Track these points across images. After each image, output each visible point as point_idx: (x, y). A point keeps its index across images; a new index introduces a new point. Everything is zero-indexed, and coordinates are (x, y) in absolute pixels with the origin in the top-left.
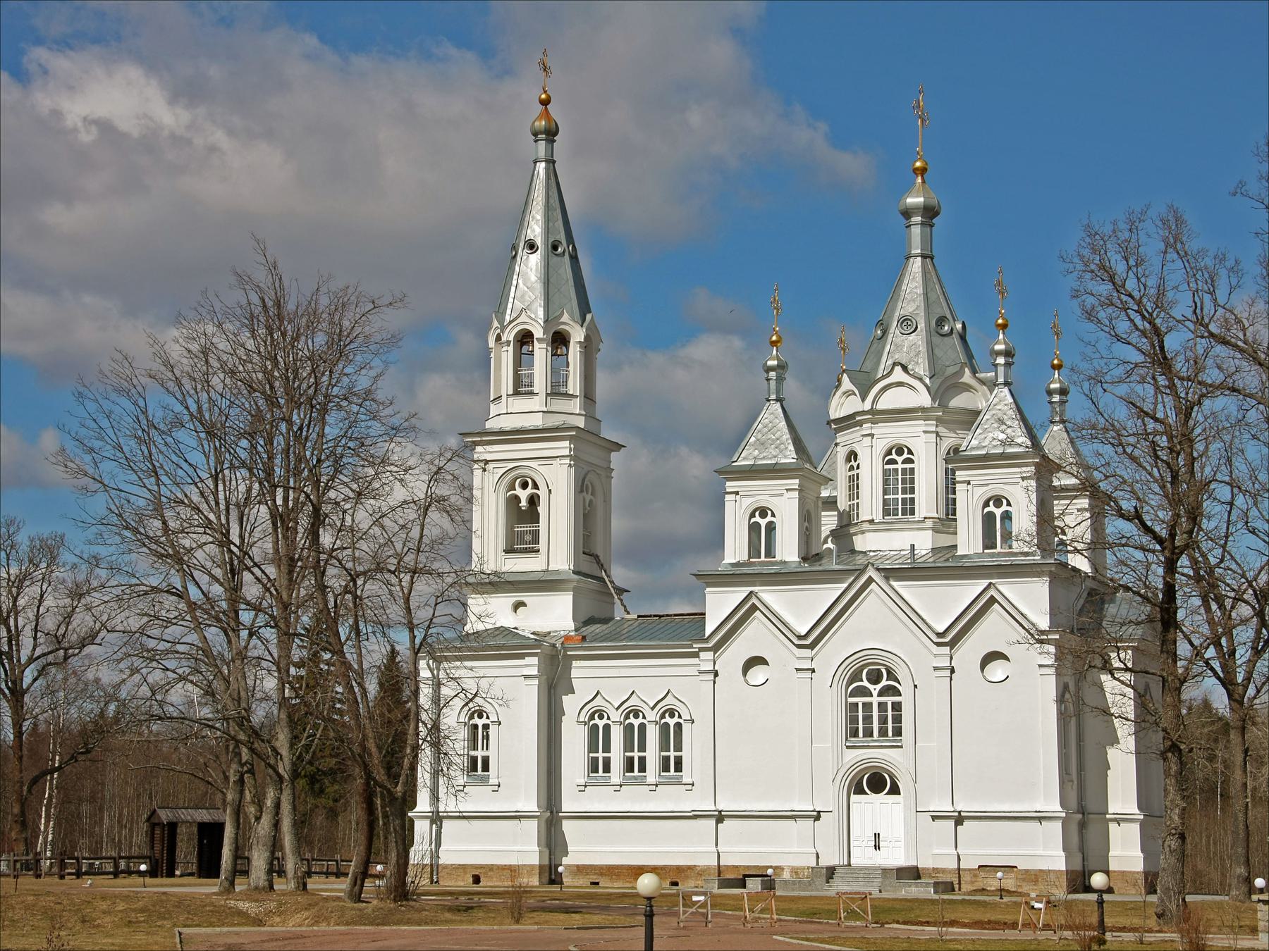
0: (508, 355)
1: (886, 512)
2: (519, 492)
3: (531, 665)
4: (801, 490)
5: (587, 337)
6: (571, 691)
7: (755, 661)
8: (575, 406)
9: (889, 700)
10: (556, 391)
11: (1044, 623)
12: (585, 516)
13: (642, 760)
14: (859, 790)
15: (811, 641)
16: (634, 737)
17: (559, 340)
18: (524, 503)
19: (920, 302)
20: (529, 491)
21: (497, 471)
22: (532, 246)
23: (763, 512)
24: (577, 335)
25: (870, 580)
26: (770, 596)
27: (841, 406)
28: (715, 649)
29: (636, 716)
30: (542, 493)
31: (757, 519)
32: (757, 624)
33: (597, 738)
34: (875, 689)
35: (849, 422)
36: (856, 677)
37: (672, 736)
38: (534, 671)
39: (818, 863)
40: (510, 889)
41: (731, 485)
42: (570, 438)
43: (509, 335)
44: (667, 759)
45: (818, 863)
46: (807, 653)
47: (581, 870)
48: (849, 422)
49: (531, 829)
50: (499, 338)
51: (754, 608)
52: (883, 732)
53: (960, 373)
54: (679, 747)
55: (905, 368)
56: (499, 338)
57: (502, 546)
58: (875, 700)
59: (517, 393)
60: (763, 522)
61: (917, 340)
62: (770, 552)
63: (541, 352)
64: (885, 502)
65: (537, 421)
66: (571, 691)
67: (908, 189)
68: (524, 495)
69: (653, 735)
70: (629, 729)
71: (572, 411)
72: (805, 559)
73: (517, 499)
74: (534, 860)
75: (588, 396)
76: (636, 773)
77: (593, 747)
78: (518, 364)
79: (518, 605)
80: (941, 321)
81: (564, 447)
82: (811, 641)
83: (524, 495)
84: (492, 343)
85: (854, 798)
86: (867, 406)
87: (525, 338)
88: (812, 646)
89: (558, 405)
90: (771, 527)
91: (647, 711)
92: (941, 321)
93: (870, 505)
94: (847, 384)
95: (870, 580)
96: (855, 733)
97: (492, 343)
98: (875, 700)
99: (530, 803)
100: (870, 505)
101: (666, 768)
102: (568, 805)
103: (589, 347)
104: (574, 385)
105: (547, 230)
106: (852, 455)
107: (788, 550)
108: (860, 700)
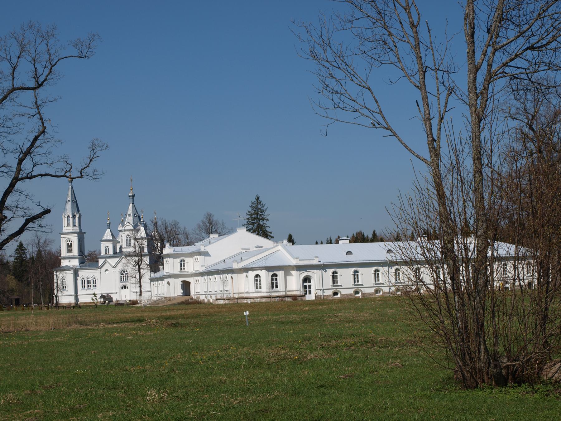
0: (66, 220)
1: (127, 245)
2: (69, 242)
3: (72, 272)
4: (113, 243)
5: (79, 216)
6: (79, 276)
7: (106, 270)
8: (78, 228)
9: (127, 275)
10: (74, 226)
11: (148, 263)
12: (80, 246)
13: (85, 286)
14: (122, 289)
15: (115, 267)
16: (89, 282)
17: (74, 217)
18: (70, 244)
19: (132, 211)
20: (70, 242)
21: (65, 239)
22: (69, 201)
23: (107, 247)
24: (78, 216)
25: (123, 257)
26: (108, 260)
27: (120, 228)
28: (101, 268)
29: (124, 272)
30: (72, 242)
31: (106, 248)
32: (107, 264)
33: (83, 282)
34: (124, 274)
35: (121, 231)
36: (122, 272)
37: (94, 282)
38: (73, 273)
39: (288, 291)
40: (149, 305)
41: (102, 243)
42: (77, 234)
43: (66, 216)
44: (94, 285)
45: (288, 291)
46: (114, 269)
47: (81, 303)
48: (121, 231)
49: (73, 297)
50: (64, 217)
51: (106, 262)
52: (126, 280)
53: (138, 223)
54: (96, 283)
55: (129, 223)
56: (64, 217)
57: (66, 251)
58: (124, 275)
59: (68, 226)
60: (107, 248)
61: (131, 218)
62: (109, 253)
63: (71, 219)
64: (127, 244)
65: (71, 231)
66: (79, 276)
67: (130, 193)
68: (69, 243)
69: (86, 282)
70: (88, 281)
71: (77, 229)
72: (114, 254)
73: (68, 244)
74: (74, 302)
75: (80, 225)
76: (89, 287)
77: (82, 284)
78: (68, 221)
79: (70, 261)
80: (135, 215)
81: (76, 235)
82: (115, 267)
83: (69, 243)
84: (63, 217)
85: (122, 290)
86: (123, 229)
87: (68, 216)
88: (115, 268)
89: (75, 228)
90: (108, 249)
91: (85, 278)
92: (135, 215)
93: (124, 245)
94: (120, 225)
95: (123, 257)
96: (121, 280)
97: (63, 217)
98: (124, 275)
99: (73, 294)
100: (124, 245)
101: (94, 286)
102: (79, 293)
103: (80, 218)
104: (77, 224)
105: (72, 198)
106: (122, 236)
107: (111, 253)
108: (122, 275)
